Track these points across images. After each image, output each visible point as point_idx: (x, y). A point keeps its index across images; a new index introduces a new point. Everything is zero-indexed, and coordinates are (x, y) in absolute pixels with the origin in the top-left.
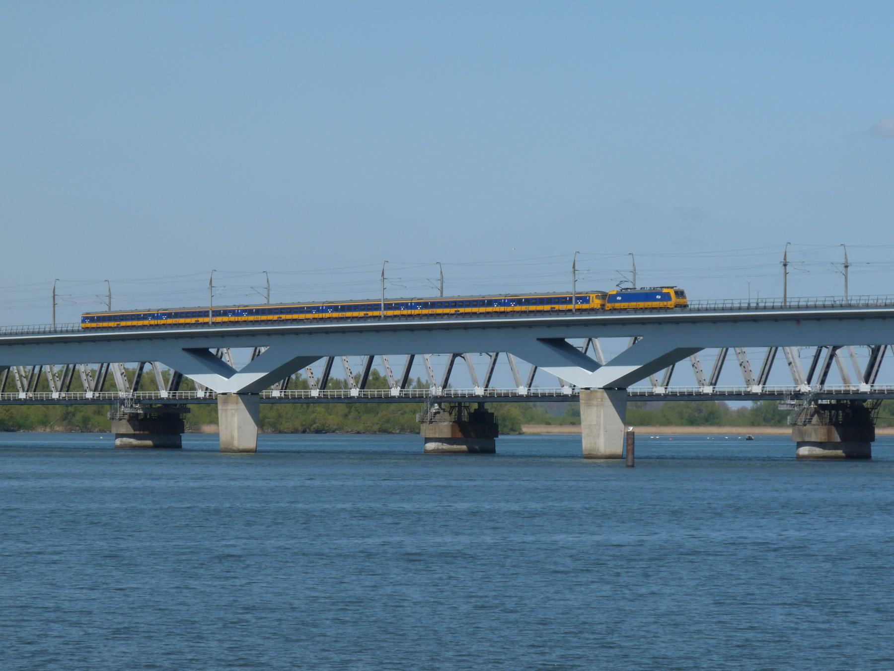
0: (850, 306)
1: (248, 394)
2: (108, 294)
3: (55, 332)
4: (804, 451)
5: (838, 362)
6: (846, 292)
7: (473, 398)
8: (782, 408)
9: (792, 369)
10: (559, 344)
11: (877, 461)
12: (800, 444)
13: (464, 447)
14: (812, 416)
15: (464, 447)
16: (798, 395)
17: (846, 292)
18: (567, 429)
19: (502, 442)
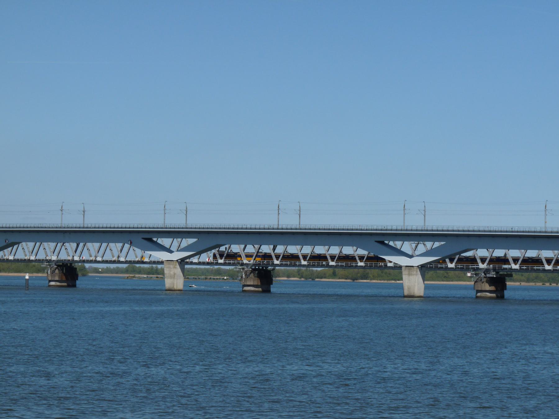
0: (187, 228)
1: (182, 262)
2: (83, 209)
4: (52, 283)
5: (95, 250)
6: (404, 223)
7: (69, 260)
8: (42, 266)
9: (50, 252)
10: (150, 240)
11: (506, 299)
12: (50, 281)
14: (55, 269)
15: (66, 284)
16: (49, 261)
17: (404, 223)
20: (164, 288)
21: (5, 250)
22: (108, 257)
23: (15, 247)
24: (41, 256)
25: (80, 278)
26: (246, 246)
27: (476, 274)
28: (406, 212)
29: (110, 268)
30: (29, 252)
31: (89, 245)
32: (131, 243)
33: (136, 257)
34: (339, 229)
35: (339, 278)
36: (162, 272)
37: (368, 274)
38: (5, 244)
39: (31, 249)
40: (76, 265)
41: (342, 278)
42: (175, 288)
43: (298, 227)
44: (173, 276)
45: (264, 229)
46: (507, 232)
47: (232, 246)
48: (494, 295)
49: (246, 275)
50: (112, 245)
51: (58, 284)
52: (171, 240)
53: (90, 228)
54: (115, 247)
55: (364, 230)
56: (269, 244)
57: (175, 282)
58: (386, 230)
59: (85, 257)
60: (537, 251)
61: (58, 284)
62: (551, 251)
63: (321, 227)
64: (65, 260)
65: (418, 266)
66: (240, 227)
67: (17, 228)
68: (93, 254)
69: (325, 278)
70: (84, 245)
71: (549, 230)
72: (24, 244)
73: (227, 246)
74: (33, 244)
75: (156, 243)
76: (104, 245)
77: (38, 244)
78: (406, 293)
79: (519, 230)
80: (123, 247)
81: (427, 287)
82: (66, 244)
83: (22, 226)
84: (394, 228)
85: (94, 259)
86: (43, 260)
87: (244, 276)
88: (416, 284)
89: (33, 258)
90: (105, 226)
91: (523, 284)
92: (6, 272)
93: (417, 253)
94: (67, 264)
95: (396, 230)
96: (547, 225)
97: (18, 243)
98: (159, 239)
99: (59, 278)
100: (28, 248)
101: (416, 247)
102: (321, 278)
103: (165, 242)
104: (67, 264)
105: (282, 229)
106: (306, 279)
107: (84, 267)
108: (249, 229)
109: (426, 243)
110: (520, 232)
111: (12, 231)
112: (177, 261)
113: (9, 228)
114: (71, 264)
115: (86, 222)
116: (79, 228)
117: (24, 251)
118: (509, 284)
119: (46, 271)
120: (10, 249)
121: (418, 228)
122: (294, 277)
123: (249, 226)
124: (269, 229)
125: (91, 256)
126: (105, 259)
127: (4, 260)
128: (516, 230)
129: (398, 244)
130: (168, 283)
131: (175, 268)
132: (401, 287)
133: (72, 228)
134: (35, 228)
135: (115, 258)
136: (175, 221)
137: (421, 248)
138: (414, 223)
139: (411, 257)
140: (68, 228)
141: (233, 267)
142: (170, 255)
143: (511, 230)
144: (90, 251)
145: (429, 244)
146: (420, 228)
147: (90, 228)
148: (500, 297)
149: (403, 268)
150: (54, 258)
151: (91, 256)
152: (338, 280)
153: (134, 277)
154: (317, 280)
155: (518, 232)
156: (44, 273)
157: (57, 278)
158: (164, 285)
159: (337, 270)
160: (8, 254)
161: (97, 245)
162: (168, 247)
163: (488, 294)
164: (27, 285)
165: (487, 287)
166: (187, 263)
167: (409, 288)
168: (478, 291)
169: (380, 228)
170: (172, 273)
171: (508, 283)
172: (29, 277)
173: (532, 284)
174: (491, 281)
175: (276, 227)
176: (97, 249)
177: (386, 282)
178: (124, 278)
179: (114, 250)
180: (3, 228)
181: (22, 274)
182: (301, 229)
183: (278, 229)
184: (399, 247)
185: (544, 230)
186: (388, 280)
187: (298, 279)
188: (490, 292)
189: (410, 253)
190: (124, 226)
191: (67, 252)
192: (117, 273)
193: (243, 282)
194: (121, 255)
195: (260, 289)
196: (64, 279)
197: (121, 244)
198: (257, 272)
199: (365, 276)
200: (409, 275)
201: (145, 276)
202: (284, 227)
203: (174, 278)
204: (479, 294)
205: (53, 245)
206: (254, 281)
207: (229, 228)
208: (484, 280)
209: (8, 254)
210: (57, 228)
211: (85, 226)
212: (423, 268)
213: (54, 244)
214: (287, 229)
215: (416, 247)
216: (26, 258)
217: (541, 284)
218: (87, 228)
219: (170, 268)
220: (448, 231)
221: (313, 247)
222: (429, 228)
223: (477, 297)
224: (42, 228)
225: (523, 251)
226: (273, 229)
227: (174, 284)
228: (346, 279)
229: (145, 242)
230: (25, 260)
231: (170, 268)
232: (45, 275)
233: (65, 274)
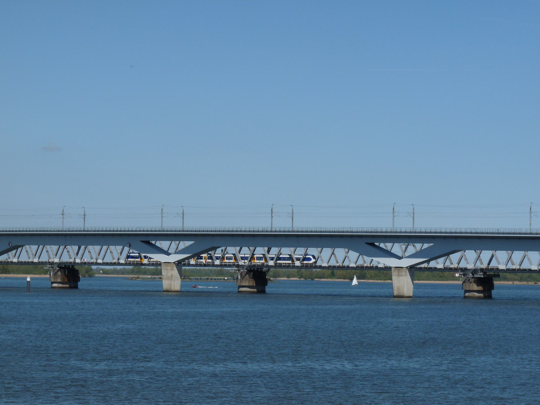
1: (179, 264)
3: (184, 231)
4: (55, 285)
6: (393, 225)
7: (71, 263)
8: (45, 268)
9: (52, 254)
10: (148, 243)
12: (53, 283)
13: (67, 286)
15: (67, 286)
16: (52, 263)
17: (393, 225)
18: (390, 281)
19: (83, 283)
20: (159, 289)
21: (10, 253)
22: (108, 259)
23: (20, 249)
24: (44, 258)
25: (269, 284)
26: (241, 248)
27: (464, 275)
28: (395, 214)
29: (117, 269)
30: (32, 254)
31: (90, 247)
32: (130, 246)
33: (337, 263)
34: (196, 231)
35: (338, 278)
36: (160, 273)
37: (365, 274)
38: (8, 247)
39: (55, 252)
40: (76, 267)
41: (340, 278)
42: (173, 289)
43: (291, 230)
44: (171, 278)
45: (258, 231)
46: (493, 233)
47: (228, 248)
48: (481, 295)
49: (241, 276)
50: (112, 248)
51: (60, 285)
52: (169, 242)
53: (90, 231)
54: (340, 253)
55: (354, 232)
56: (263, 246)
57: (173, 284)
58: (376, 232)
59: (87, 259)
60: (523, 252)
61: (60, 285)
62: (505, 252)
63: (313, 230)
64: (67, 263)
65: (407, 267)
66: (235, 229)
67: (19, 231)
68: (94, 256)
69: (324, 278)
70: (85, 248)
71: (535, 231)
72: (27, 247)
73: (223, 248)
74: (36, 247)
75: (154, 246)
76: (105, 247)
77: (41, 247)
78: (396, 293)
79: (505, 232)
80: (123, 250)
81: (416, 286)
82: (68, 247)
83: (28, 230)
84: (384, 230)
85: (95, 261)
86: (46, 262)
87: (239, 277)
88: (406, 285)
89: (36, 260)
90: (104, 229)
91: (516, 283)
92: (15, 274)
93: (407, 254)
94: (69, 266)
95: (406, 232)
96: (532, 227)
97: (23, 246)
98: (158, 242)
99: (61, 279)
100: (52, 251)
101: (406, 248)
102: (321, 278)
103: (163, 244)
104: (69, 266)
105: (276, 231)
106: (306, 279)
107: (91, 269)
108: (130, 231)
109: (416, 244)
110: (359, 232)
111: (58, 235)
112: (174, 263)
113: (13, 231)
114: (73, 266)
115: (395, 226)
116: (80, 231)
117: (28, 254)
118: (496, 283)
119: (49, 273)
120: (14, 252)
121: (407, 230)
122: (294, 277)
123: (243, 229)
124: (262, 231)
125: (92, 258)
126: (105, 261)
127: (8, 262)
128: (502, 231)
129: (388, 246)
130: (166, 284)
131: (172, 269)
132: (391, 286)
133: (73, 231)
134: (54, 231)
135: (115, 261)
136: (173, 224)
137: (411, 250)
138: (404, 225)
139: (400, 258)
140: (69, 231)
141: (153, 267)
142: (168, 256)
143: (497, 231)
144: (91, 254)
145: (418, 246)
146: (409, 230)
147: (90, 231)
148: (488, 296)
149: (393, 269)
150: (56, 260)
151: (92, 258)
152: (337, 280)
153: (138, 278)
154: (316, 279)
155: (503, 233)
156: (46, 274)
157: (59, 280)
158: (162, 285)
159: (335, 271)
160: (12, 257)
161: (98, 248)
162: (166, 249)
163: (476, 294)
164: (28, 287)
165: (475, 287)
166: (184, 265)
167: (398, 289)
168: (466, 291)
169: (370, 230)
170: (169, 275)
171: (495, 282)
172: (31, 279)
173: (524, 283)
174: (479, 281)
175: (269, 229)
176: (98, 251)
177: (382, 281)
178: (128, 279)
179: (116, 253)
180: (3, 231)
181: (24, 276)
182: (293, 232)
183: (271, 231)
184: (389, 249)
185: (529, 232)
186: (384, 280)
187: (298, 279)
188: (478, 292)
189: (400, 254)
190: (123, 229)
191: (69, 255)
192: (123, 274)
193: (239, 283)
194: (121, 257)
195: (255, 290)
196: (66, 280)
197: (121, 247)
198: (252, 273)
199: (362, 276)
200: (399, 275)
201: (149, 277)
202: (278, 229)
203: (171, 279)
204: (467, 294)
205: (55, 248)
206: (249, 282)
207: (224, 231)
208: (472, 280)
209: (12, 257)
210: (58, 231)
211: (86, 229)
212: (412, 269)
213: (57, 247)
214: (280, 231)
215: (406, 248)
216: (30, 260)
217: (533, 283)
218: (87, 231)
219: (167, 269)
220: (436, 233)
221: (306, 249)
222: (418, 230)
223: (465, 297)
224: (44, 231)
225: (510, 252)
226: (267, 231)
227: (171, 285)
228: (345, 279)
229: (143, 244)
230: (29, 262)
231: (167, 269)
232: (48, 276)
233: (67, 276)
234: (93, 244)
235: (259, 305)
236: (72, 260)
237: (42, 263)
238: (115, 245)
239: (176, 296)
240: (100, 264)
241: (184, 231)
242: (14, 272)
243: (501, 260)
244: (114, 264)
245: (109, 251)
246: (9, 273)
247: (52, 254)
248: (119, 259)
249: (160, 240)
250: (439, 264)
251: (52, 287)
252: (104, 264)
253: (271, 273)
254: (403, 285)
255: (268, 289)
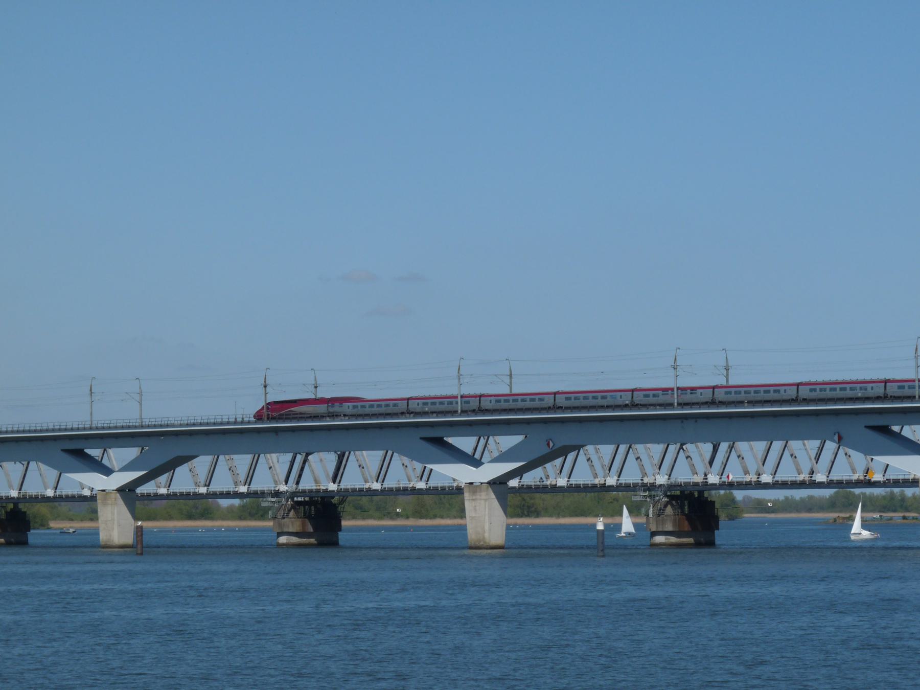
3: (142, 427)
4: (659, 539)
7: (696, 484)
10: (884, 430)
12: (654, 534)
13: (691, 540)
15: (691, 540)
16: (651, 487)
19: (34, 536)
21: (548, 465)
22: (787, 473)
23: (571, 456)
24: (631, 476)
31: (742, 446)
32: (840, 438)
34: (116, 428)
38: (545, 450)
39: (657, 460)
40: (714, 495)
50: (795, 444)
51: (673, 540)
59: (734, 474)
61: (673, 540)
64: (687, 484)
68: (753, 466)
70: (731, 448)
75: (898, 437)
76: (777, 445)
80: (821, 449)
82: (689, 447)
89: (611, 481)
92: (551, 516)
97: (578, 448)
98: (906, 428)
99: (674, 526)
104: (692, 494)
107: (733, 500)
114: (701, 493)
119: (643, 510)
120: (558, 462)
125: (746, 472)
126: (780, 477)
127: (545, 487)
135: (858, 476)
144: (741, 464)
157: (669, 527)
161: (760, 446)
172: (605, 525)
179: (805, 458)
191: (693, 464)
192: (810, 510)
196: (686, 527)
197: (817, 443)
216: (597, 481)
233: (688, 518)
234: (749, 439)
235: (324, 568)
236: (699, 479)
237: (627, 487)
238: (803, 439)
239: (504, 556)
240: (766, 486)
241: (142, 427)
242: (547, 512)
243: (364, 470)
244: (802, 485)
245: (787, 453)
246: (538, 514)
247: (655, 464)
248: (812, 472)
249: (910, 424)
250: (553, 475)
251: (280, 546)
252: (776, 485)
253: (347, 508)
254: (486, 521)
255: (720, 536)
